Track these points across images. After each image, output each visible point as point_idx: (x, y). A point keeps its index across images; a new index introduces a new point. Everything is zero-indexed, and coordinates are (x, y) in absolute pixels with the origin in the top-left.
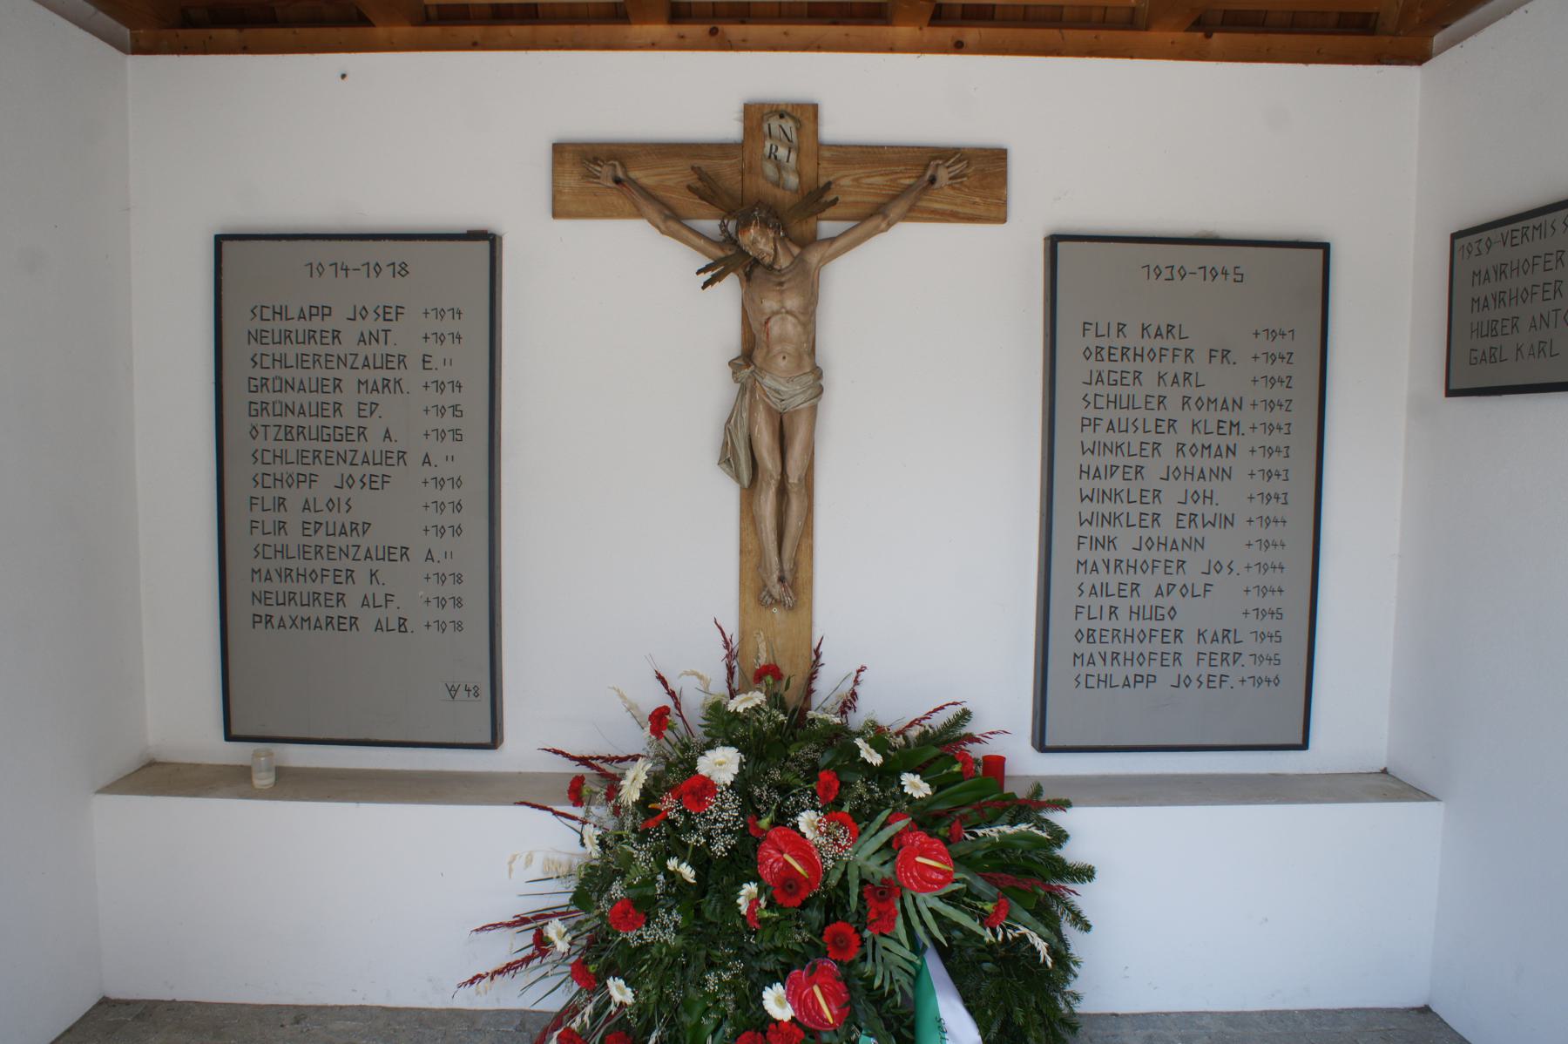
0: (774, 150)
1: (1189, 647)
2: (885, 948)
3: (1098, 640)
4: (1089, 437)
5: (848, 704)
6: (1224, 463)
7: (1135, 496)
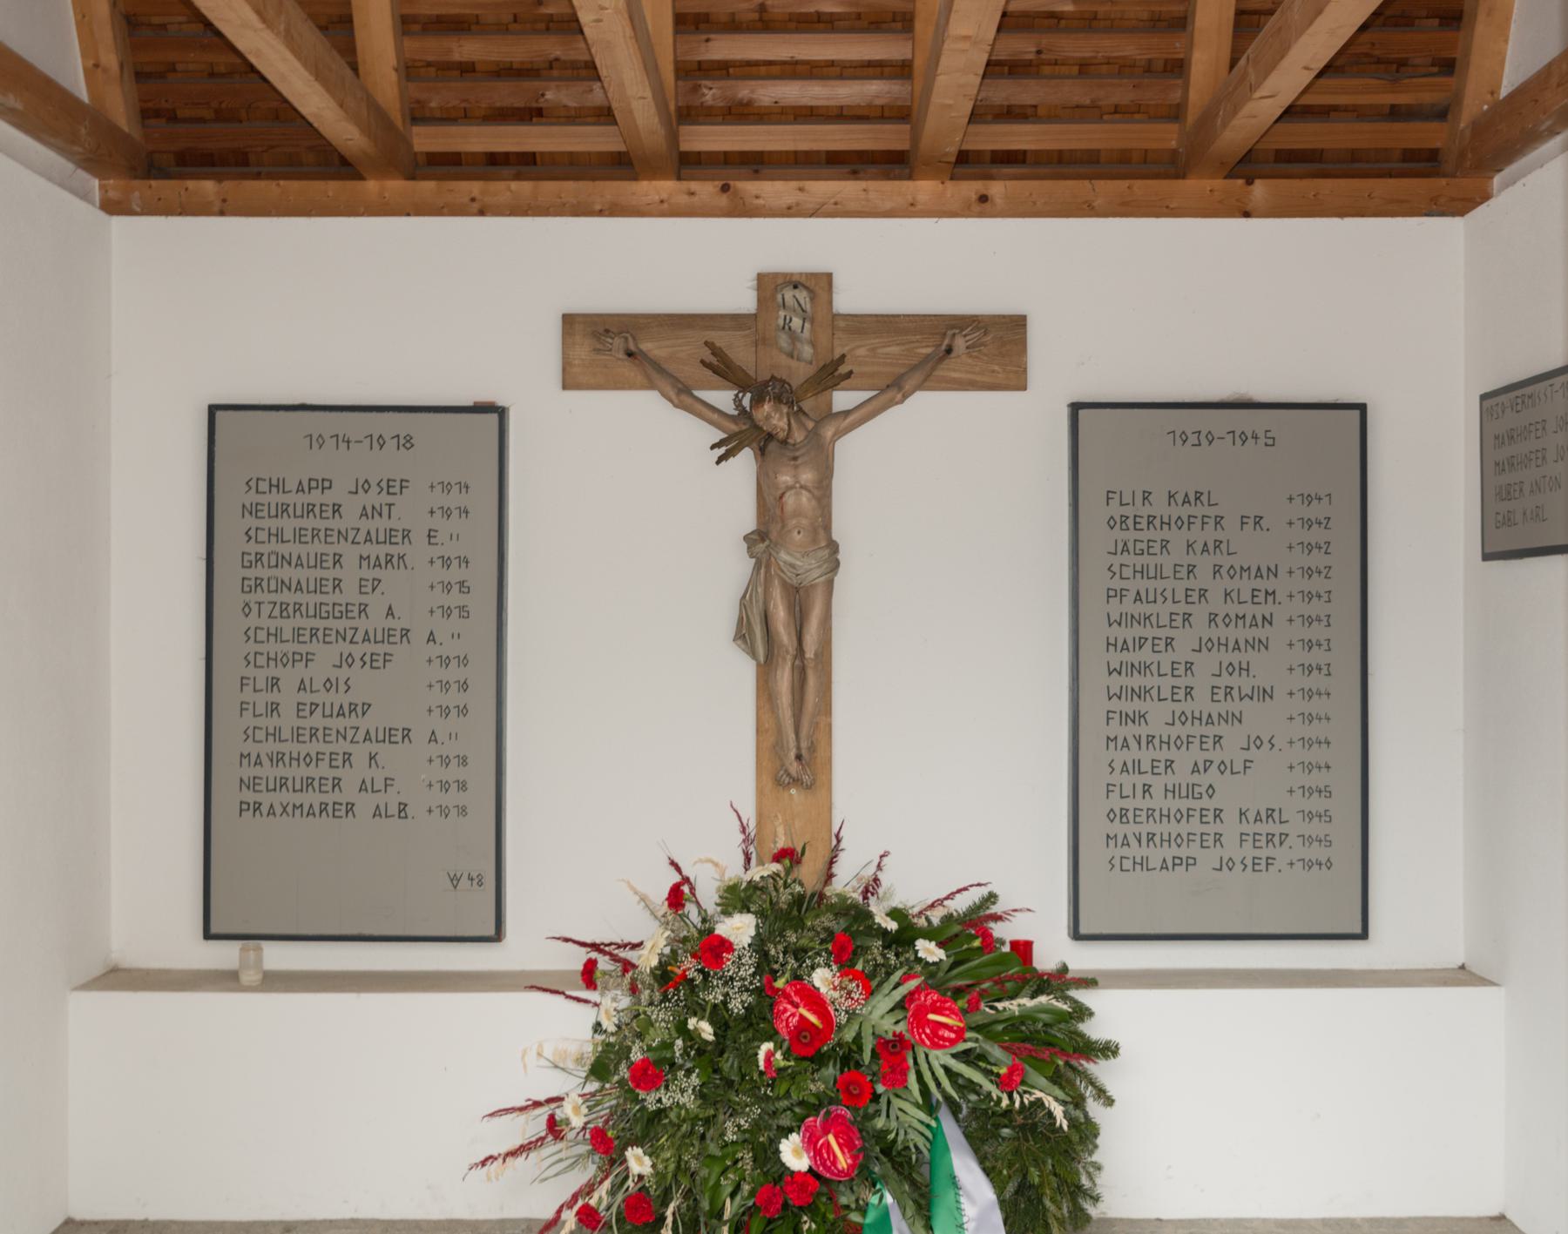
0: (788, 321)
1: (1231, 828)
2: (901, 1110)
3: (1131, 820)
4: (1115, 608)
5: (871, 888)
6: (1260, 633)
7: (1166, 669)
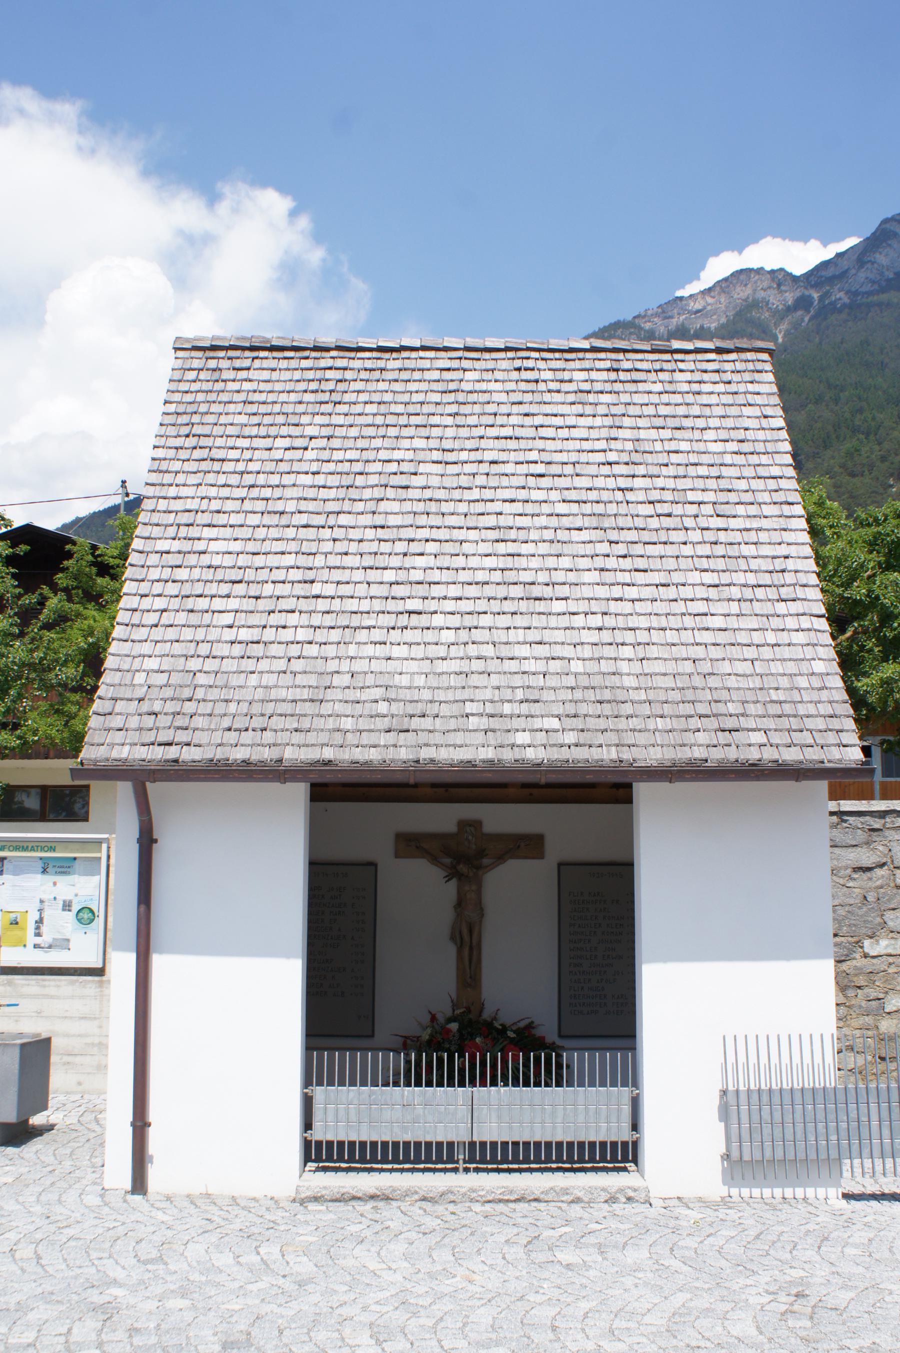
5: (495, 1019)
